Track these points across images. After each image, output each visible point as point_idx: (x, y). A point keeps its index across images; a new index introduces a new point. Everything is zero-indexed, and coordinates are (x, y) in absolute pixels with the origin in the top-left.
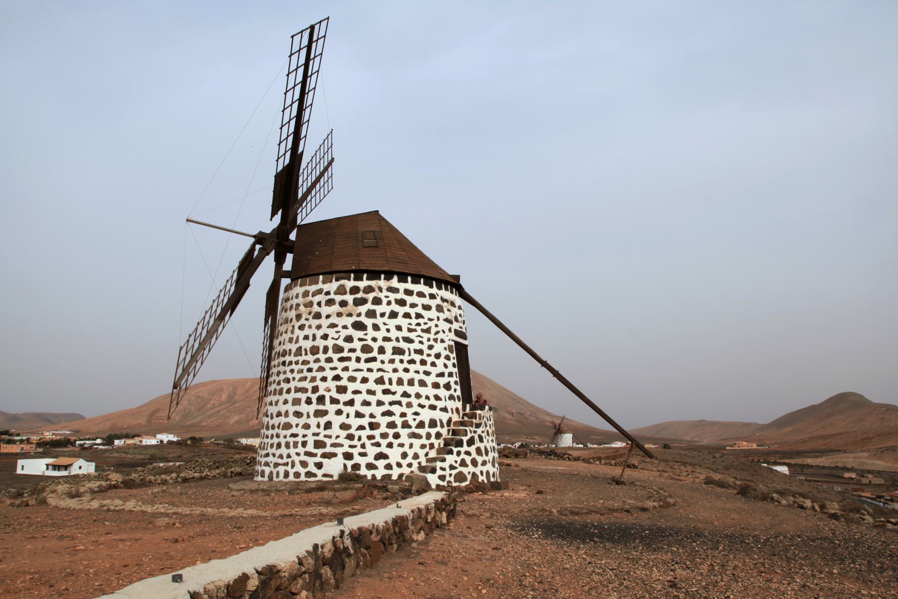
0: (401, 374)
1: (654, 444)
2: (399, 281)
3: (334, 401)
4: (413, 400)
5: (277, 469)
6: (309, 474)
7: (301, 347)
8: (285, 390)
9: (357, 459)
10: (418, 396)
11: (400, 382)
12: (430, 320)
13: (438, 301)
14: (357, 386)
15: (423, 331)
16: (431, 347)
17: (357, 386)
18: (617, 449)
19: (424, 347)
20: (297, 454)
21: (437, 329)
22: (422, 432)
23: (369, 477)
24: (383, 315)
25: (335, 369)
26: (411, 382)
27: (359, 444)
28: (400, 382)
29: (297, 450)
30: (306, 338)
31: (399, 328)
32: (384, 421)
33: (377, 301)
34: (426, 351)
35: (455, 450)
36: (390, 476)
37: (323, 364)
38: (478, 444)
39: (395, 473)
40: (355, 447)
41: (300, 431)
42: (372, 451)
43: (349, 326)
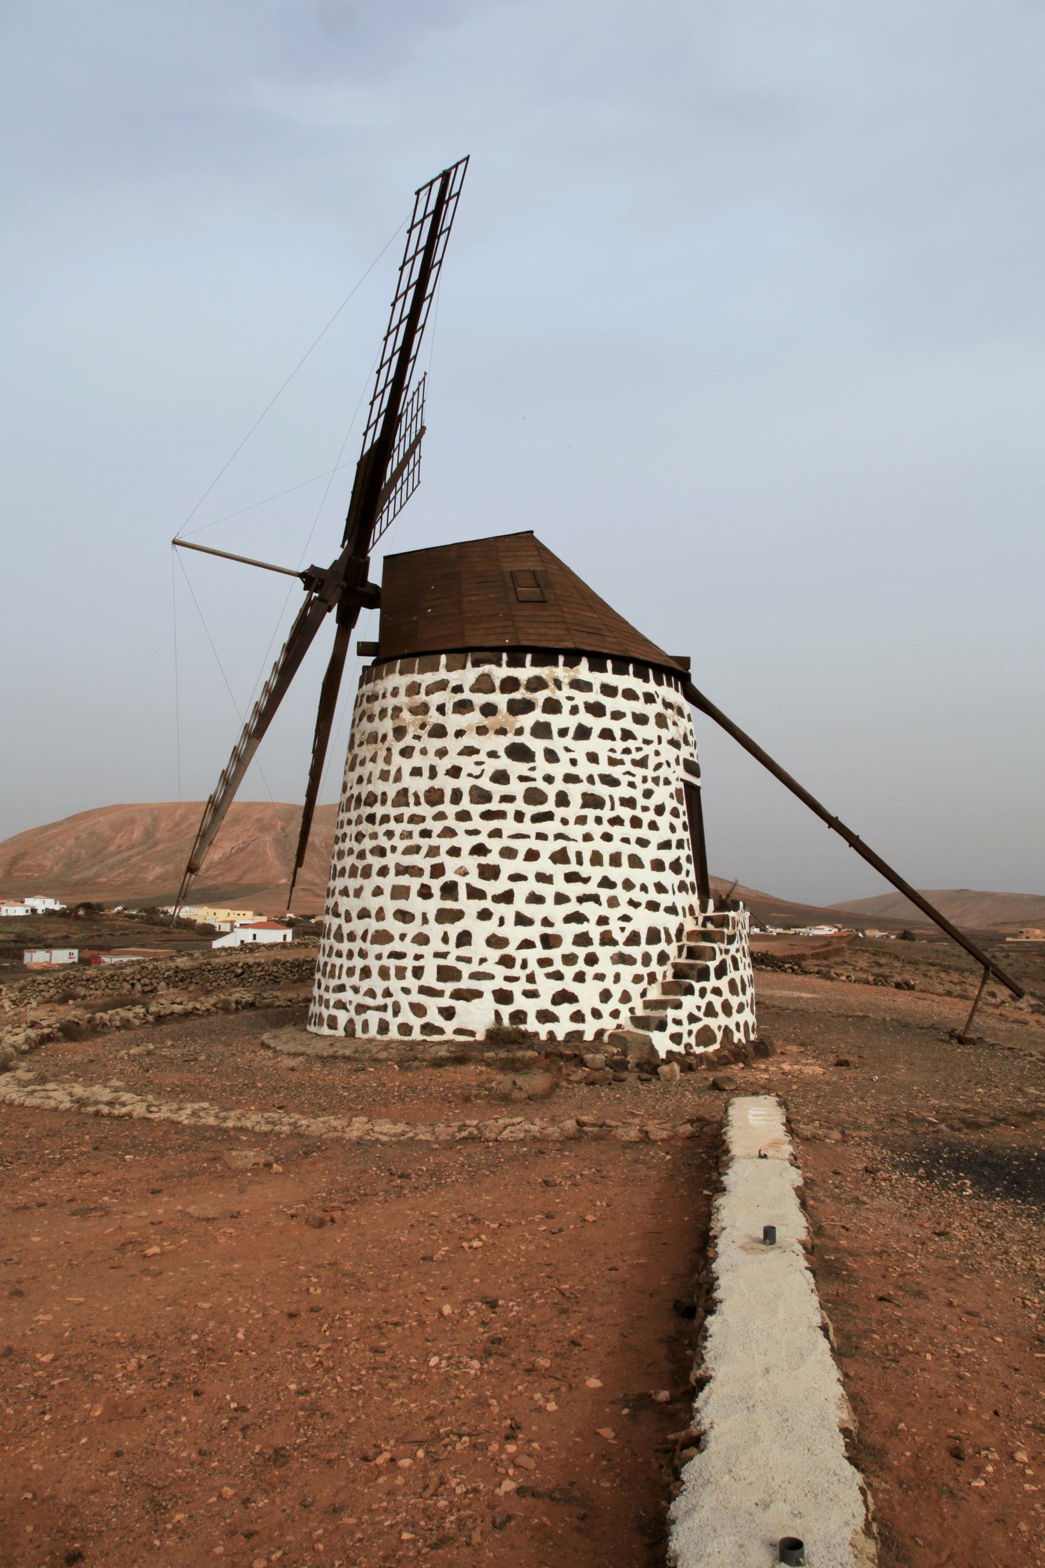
0: (598, 844)
1: (880, 929)
2: (592, 669)
3: (475, 894)
4: (619, 892)
5: (364, 1016)
6: (428, 1028)
7: (405, 791)
8: (375, 870)
9: (521, 1003)
10: (628, 885)
11: (596, 859)
12: (647, 742)
13: (658, 707)
14: (518, 865)
15: (635, 763)
16: (648, 794)
17: (518, 865)
18: (827, 940)
19: (637, 794)
20: (404, 991)
21: (658, 760)
22: (636, 952)
23: (543, 1037)
24: (563, 733)
25: (475, 832)
26: (615, 860)
27: (523, 974)
28: (596, 859)
29: (403, 983)
30: (416, 772)
31: (593, 758)
32: (568, 932)
33: (552, 706)
34: (641, 802)
35: (697, 986)
36: (580, 1034)
37: (451, 822)
38: (732, 974)
39: (589, 1028)
40: (515, 979)
41: (410, 948)
42: (547, 988)
43: (501, 753)
